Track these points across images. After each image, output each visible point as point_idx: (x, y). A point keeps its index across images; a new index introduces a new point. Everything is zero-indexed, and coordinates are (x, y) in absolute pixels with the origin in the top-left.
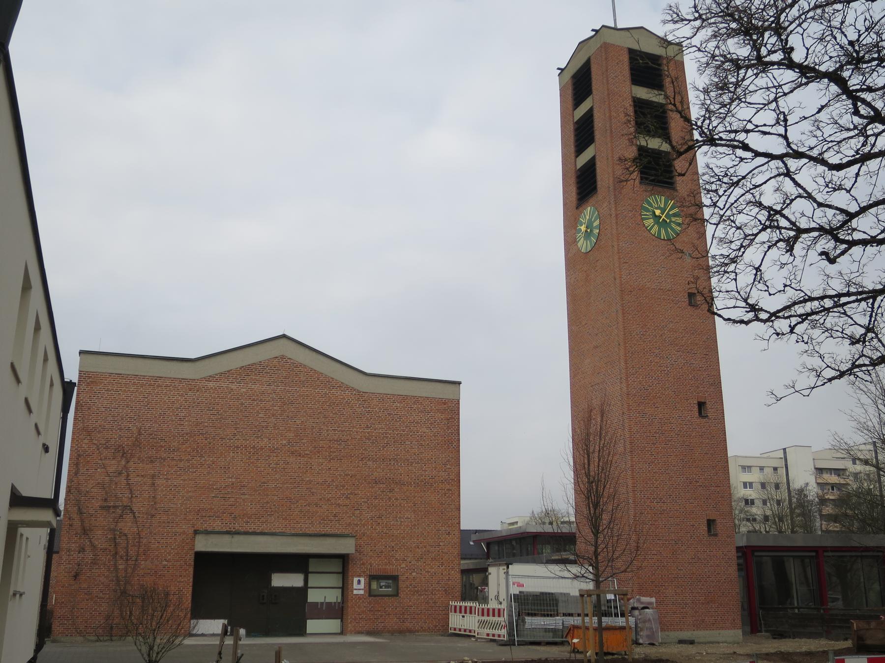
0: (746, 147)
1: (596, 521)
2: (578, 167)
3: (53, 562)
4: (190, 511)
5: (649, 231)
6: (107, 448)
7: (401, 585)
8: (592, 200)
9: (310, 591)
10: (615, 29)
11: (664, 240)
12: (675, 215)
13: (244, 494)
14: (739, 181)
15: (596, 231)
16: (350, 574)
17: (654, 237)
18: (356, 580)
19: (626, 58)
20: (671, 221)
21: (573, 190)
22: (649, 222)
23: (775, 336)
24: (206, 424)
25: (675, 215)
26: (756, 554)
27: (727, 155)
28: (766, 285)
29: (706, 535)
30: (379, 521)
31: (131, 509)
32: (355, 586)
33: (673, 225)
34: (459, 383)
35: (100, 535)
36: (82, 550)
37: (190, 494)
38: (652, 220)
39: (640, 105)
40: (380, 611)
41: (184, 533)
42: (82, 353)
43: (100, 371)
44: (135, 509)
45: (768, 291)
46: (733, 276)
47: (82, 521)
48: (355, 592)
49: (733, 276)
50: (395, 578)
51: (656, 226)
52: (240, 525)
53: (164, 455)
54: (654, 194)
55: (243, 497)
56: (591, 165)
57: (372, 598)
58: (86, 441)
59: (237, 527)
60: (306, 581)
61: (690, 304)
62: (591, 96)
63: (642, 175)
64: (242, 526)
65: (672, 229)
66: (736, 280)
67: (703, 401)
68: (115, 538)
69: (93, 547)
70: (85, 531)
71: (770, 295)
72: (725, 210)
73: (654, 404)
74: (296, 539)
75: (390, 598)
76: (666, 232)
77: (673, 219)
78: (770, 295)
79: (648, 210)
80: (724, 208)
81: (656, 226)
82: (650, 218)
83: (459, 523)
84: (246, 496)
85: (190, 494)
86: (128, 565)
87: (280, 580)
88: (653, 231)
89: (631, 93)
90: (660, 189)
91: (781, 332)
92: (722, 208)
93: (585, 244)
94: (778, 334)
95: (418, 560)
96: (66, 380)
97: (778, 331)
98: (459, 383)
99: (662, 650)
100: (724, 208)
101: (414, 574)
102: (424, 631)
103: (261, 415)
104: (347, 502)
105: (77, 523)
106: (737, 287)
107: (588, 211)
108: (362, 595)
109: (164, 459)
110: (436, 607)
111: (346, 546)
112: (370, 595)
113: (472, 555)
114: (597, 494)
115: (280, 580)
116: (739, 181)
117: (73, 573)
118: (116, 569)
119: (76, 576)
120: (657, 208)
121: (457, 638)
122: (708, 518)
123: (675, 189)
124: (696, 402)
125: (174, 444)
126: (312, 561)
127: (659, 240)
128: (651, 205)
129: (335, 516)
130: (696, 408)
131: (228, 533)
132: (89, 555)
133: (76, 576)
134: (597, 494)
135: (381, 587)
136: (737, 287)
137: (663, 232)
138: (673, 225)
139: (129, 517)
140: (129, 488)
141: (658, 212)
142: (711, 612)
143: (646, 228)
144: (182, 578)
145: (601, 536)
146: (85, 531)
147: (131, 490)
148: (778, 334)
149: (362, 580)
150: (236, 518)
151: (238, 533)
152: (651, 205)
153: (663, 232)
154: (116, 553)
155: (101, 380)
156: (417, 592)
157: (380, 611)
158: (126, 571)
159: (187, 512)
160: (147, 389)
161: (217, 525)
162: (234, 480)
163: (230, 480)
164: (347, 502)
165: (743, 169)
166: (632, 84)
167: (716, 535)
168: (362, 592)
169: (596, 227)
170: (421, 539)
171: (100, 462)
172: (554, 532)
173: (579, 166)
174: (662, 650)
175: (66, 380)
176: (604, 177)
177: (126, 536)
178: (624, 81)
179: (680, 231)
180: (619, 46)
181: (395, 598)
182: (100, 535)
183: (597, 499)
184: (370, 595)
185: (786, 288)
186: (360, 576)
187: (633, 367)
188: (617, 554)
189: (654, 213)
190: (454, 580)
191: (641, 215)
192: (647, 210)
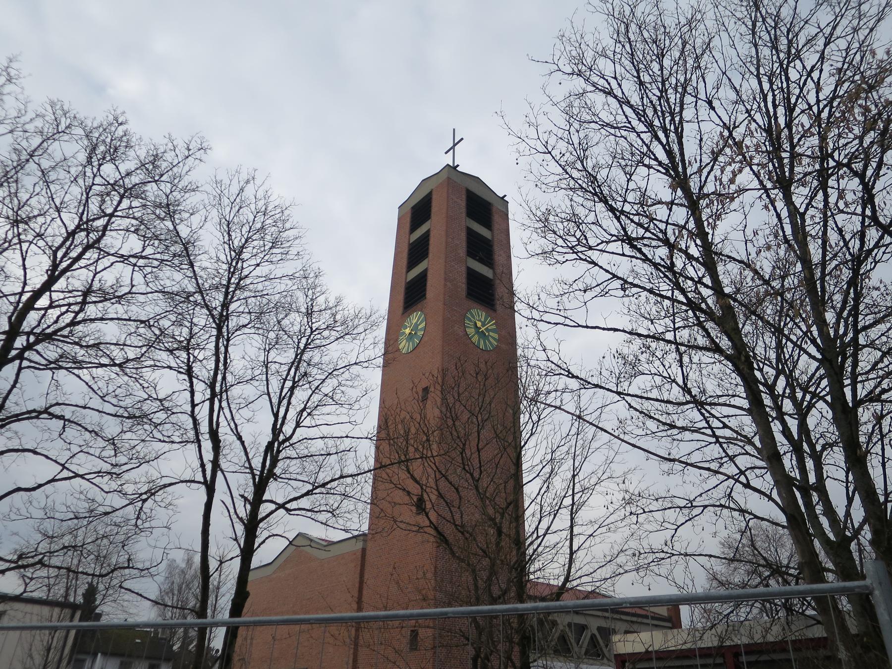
2: (408, 280)
11: (482, 349)
12: (492, 331)
15: (420, 333)
19: (464, 192)
20: (489, 335)
21: (401, 297)
25: (492, 331)
33: (491, 340)
38: (473, 330)
39: (472, 277)
51: (476, 336)
56: (423, 276)
62: (430, 221)
76: (485, 343)
77: (491, 334)
79: (470, 321)
81: (476, 336)
93: (407, 345)
99: (31, 594)
107: (416, 318)
121: (887, 647)
123: (495, 311)
137: (482, 342)
138: (491, 340)
141: (479, 324)
166: (468, 255)
169: (421, 330)
173: (409, 279)
174: (31, 594)
176: (434, 288)
185: (628, 200)
189: (476, 324)
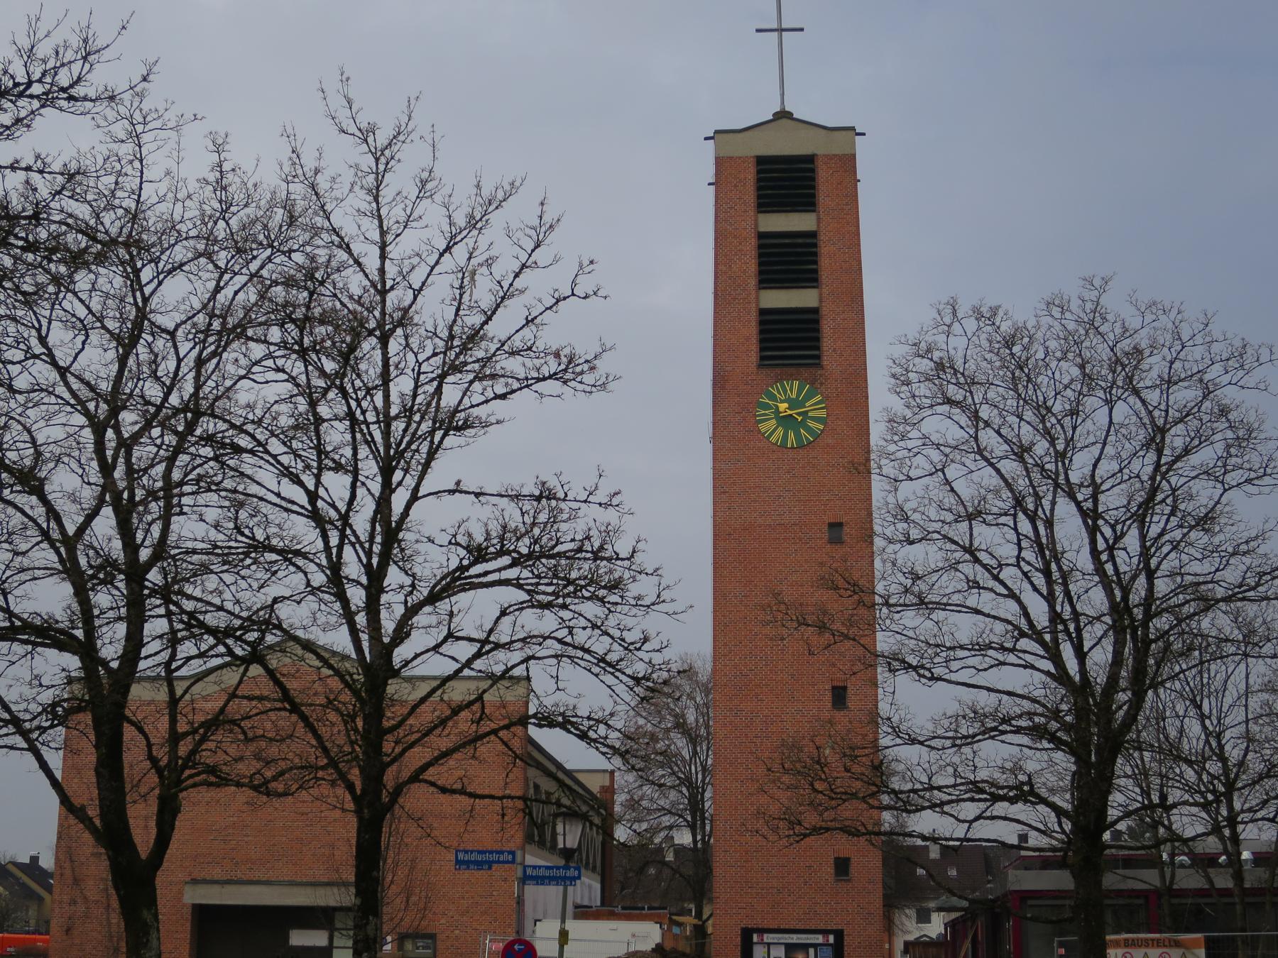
3: (787, 927)
7: (440, 945)
9: (335, 951)
13: (247, 836)
17: (775, 447)
22: (768, 426)
26: (1030, 902)
33: (811, 424)
36: (73, 902)
37: (187, 837)
38: (774, 421)
47: (73, 870)
50: (432, 937)
51: (780, 428)
54: (781, 380)
55: (246, 839)
58: (76, 780)
59: (239, 874)
60: (331, 939)
65: (809, 430)
69: (85, 898)
70: (76, 881)
73: (757, 695)
76: (798, 435)
81: (780, 428)
84: (250, 838)
85: (187, 837)
87: (300, 938)
88: (773, 439)
89: (756, 225)
90: (792, 370)
105: (68, 872)
115: (300, 938)
117: (65, 928)
118: (109, 924)
119: (68, 931)
120: (782, 402)
122: (836, 855)
124: (828, 687)
126: (338, 915)
128: (773, 398)
132: (81, 908)
133: (68, 931)
135: (418, 948)
146: (76, 881)
152: (773, 398)
153: (791, 435)
154: (109, 906)
161: (217, 873)
162: (235, 819)
178: (745, 211)
179: (822, 431)
180: (740, 158)
187: (725, 645)
191: (755, 416)
192: (767, 407)
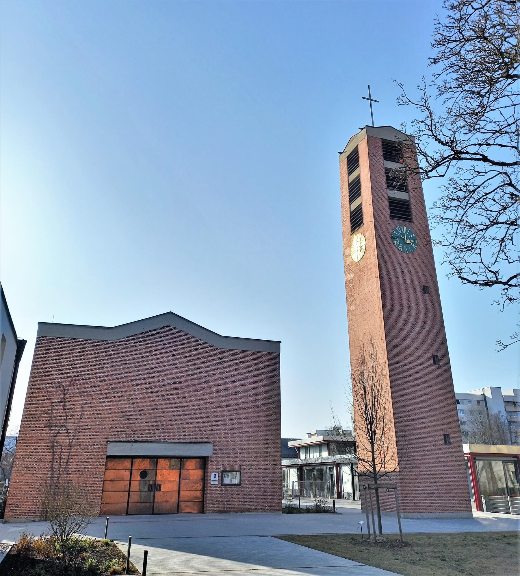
0: (485, 159)
1: (372, 435)
4: (105, 428)
5: (397, 248)
6: (52, 386)
8: (361, 229)
10: (373, 127)
14: (476, 189)
16: (209, 470)
17: (400, 252)
18: (213, 474)
19: (380, 145)
23: (508, 301)
24: (118, 370)
27: (468, 170)
28: (506, 255)
29: (443, 445)
30: (229, 433)
31: (66, 427)
32: (213, 478)
34: (280, 342)
35: (43, 445)
40: (229, 496)
41: (100, 443)
42: (40, 323)
43: (50, 335)
44: (68, 427)
45: (508, 260)
46: (478, 251)
48: (212, 483)
49: (478, 251)
51: (401, 245)
52: (138, 437)
53: (89, 390)
57: (224, 487)
59: (136, 438)
61: (425, 293)
63: (391, 214)
64: (139, 438)
66: (480, 254)
67: (436, 355)
68: (53, 447)
71: (509, 263)
72: (466, 209)
74: (174, 445)
75: (236, 487)
78: (509, 263)
80: (465, 208)
81: (401, 245)
82: (398, 240)
83: (280, 435)
84: (143, 417)
86: (61, 466)
91: (512, 298)
92: (464, 208)
94: (510, 300)
95: (253, 460)
96: (18, 339)
97: (510, 297)
98: (280, 342)
100: (465, 208)
101: (251, 470)
102: (258, 510)
103: (154, 364)
104: (208, 420)
106: (481, 259)
108: (217, 485)
109: (90, 393)
110: (266, 493)
111: (206, 450)
112: (222, 485)
113: (289, 455)
114: (372, 416)
116: (476, 189)
125: (97, 383)
127: (403, 253)
129: (200, 430)
130: (432, 360)
131: (129, 442)
134: (372, 416)
136: (481, 259)
137: (405, 248)
139: (63, 433)
140: (65, 413)
142: (450, 499)
143: (395, 246)
144: (97, 475)
145: (376, 446)
147: (66, 414)
148: (510, 300)
149: (217, 474)
150: (135, 432)
151: (136, 442)
155: (51, 341)
156: (253, 482)
157: (229, 496)
158: (59, 470)
159: (103, 428)
160: (81, 347)
162: (135, 406)
163: (133, 406)
164: (208, 420)
165: (478, 181)
166: (384, 160)
167: (450, 444)
168: (217, 483)
170: (256, 446)
171: (47, 395)
172: (343, 441)
175: (18, 339)
177: (61, 445)
181: (239, 487)
182: (43, 445)
183: (372, 419)
184: (222, 485)
186: (215, 472)
188: (387, 459)
190: (278, 474)
